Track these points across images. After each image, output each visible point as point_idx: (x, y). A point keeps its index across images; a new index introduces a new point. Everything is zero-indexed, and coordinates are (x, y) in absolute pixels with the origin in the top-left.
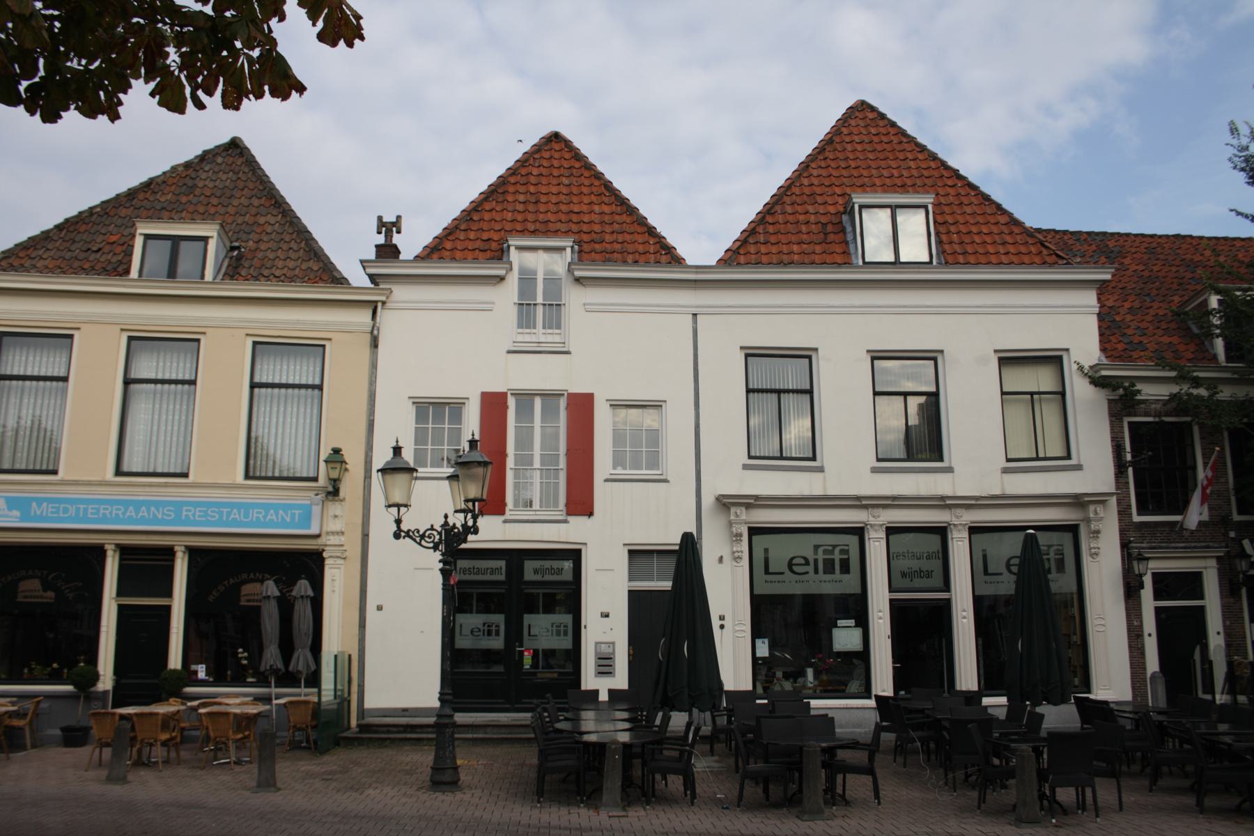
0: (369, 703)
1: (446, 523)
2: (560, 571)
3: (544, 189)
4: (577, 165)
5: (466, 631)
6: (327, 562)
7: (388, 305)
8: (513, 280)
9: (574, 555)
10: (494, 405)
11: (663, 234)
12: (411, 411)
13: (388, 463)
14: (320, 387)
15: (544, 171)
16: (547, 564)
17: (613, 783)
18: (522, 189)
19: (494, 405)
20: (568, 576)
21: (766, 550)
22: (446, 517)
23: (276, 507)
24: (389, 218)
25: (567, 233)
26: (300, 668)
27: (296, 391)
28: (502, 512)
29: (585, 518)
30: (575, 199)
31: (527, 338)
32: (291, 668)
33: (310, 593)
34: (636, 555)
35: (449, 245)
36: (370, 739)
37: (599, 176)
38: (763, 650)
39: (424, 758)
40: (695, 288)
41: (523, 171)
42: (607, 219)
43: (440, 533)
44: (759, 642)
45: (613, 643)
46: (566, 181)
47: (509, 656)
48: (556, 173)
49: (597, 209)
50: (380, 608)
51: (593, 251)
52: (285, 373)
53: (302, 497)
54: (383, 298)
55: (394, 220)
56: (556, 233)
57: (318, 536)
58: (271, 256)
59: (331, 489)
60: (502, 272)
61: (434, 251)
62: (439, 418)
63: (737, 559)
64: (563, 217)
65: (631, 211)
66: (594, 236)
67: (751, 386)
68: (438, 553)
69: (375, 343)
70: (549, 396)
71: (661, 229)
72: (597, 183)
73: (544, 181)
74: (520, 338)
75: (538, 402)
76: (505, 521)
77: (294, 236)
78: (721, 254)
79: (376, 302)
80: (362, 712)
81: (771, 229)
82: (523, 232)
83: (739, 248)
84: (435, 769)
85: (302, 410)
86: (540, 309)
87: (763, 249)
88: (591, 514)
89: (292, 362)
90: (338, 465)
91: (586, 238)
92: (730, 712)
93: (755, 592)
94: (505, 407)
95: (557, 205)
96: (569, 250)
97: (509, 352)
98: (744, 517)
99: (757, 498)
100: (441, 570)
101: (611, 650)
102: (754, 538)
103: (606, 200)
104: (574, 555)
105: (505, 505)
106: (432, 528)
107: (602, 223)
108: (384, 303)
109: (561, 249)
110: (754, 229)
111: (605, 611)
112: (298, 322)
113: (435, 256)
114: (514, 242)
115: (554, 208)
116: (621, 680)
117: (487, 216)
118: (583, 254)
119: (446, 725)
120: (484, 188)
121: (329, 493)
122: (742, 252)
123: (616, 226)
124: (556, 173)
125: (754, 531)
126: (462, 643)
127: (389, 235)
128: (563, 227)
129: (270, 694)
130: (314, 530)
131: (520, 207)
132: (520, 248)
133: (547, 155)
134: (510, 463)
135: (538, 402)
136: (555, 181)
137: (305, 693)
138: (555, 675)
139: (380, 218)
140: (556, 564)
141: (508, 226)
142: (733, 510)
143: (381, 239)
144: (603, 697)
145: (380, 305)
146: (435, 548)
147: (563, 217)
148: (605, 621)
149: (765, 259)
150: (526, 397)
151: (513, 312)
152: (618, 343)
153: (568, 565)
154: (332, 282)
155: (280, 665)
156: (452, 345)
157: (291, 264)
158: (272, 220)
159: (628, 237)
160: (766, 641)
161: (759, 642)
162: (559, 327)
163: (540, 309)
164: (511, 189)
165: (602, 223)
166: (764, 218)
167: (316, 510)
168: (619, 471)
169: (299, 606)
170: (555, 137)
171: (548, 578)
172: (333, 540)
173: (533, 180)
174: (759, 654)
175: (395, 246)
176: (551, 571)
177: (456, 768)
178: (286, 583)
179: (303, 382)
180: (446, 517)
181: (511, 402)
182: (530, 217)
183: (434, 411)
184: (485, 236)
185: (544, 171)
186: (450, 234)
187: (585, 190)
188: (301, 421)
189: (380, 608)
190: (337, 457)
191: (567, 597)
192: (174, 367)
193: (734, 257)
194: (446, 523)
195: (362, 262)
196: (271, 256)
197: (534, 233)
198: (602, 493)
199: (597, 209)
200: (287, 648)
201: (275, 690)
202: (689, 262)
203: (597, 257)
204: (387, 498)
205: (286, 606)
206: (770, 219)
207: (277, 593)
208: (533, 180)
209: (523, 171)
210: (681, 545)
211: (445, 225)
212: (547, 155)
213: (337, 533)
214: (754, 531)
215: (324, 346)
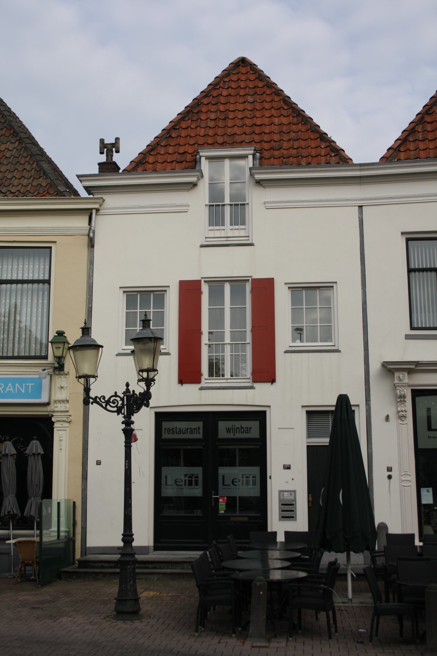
0: (90, 543)
1: (128, 390)
2: (248, 430)
3: (232, 108)
4: (261, 84)
5: (170, 481)
6: (55, 425)
7: (101, 212)
8: (204, 187)
9: (260, 417)
10: (190, 291)
11: (333, 138)
12: (122, 299)
13: (77, 341)
14: (48, 282)
15: (233, 92)
16: (238, 424)
17: (258, 616)
18: (213, 108)
19: (190, 291)
20: (255, 434)
21: (429, 410)
22: (127, 385)
23: (14, 381)
24: (109, 140)
25: (250, 143)
26: (32, 514)
27: (30, 285)
28: (199, 382)
29: (270, 384)
30: (258, 114)
31: (217, 234)
32: (25, 514)
33: (41, 451)
34: (313, 415)
35: (151, 159)
36: (86, 573)
37: (279, 92)
38: (428, 497)
39: (112, 589)
40: (360, 184)
41: (215, 93)
42: (285, 129)
43: (122, 399)
44: (424, 491)
45: (295, 491)
46: (250, 99)
47: (205, 503)
48: (242, 92)
49: (276, 121)
50: (99, 463)
51: (273, 157)
52: (20, 271)
53: (32, 371)
54: (97, 206)
55: (114, 142)
56: (241, 144)
57: (48, 404)
58: (9, 176)
59: (57, 365)
60: (194, 179)
61: (140, 164)
62: (145, 304)
63: (402, 417)
64: (248, 130)
65: (306, 121)
66: (273, 144)
67: (412, 267)
68: (121, 416)
69: (91, 244)
70: (237, 283)
71: (332, 135)
72: (277, 99)
73: (232, 100)
74: (211, 234)
75: (227, 288)
76: (201, 389)
77: (28, 159)
78: (383, 152)
79: (92, 209)
80: (85, 549)
81: (429, 128)
82: (214, 145)
83: (399, 146)
84: (120, 601)
85: (35, 301)
86: (227, 209)
87: (422, 146)
88: (273, 381)
89: (26, 263)
90: (61, 346)
91: (266, 146)
92: (385, 552)
93: (420, 447)
94: (199, 293)
95: (246, 121)
96: (251, 157)
97: (202, 246)
98: (406, 381)
99: (417, 363)
100: (123, 430)
101: (292, 498)
102: (417, 399)
103: (285, 113)
104: (260, 417)
105: (200, 375)
106: (116, 395)
107: (281, 132)
108: (97, 210)
109: (244, 157)
110: (413, 128)
111: (287, 463)
112: (29, 229)
113: (140, 169)
114: (204, 153)
115: (239, 123)
116: (301, 524)
117: (183, 133)
118: (264, 160)
119: (127, 563)
120: (181, 109)
121: (55, 369)
122: (402, 149)
123: (293, 135)
124: (242, 92)
125: (416, 393)
126: (169, 491)
127: (110, 155)
128: (247, 138)
129: (9, 535)
130: (44, 399)
131: (212, 124)
132: (208, 158)
133: (235, 78)
134: (205, 339)
135: (227, 288)
136: (241, 100)
137: (32, 535)
138: (246, 519)
139: (102, 141)
140: (246, 424)
141: (201, 140)
142: (396, 374)
143: (103, 158)
144: (281, 538)
145: (94, 212)
146: (119, 411)
147: (248, 130)
148: (287, 470)
149: (422, 154)
150: (216, 284)
151: (204, 214)
152: (295, 235)
153: (255, 425)
154: (57, 195)
155: (16, 511)
156: (154, 243)
157: (25, 182)
158: (11, 147)
159: (303, 144)
160: (431, 490)
161: (424, 491)
162: (243, 223)
163: (227, 209)
164: (204, 109)
165: (281, 132)
166: (422, 118)
167: (46, 382)
168: (298, 343)
169: (31, 462)
170: (242, 62)
171: (238, 435)
172: (60, 407)
173: (223, 100)
174: (424, 502)
175: (115, 163)
176: (241, 430)
177: (137, 600)
178: (21, 444)
179: (36, 278)
180: (127, 385)
181: (205, 288)
182: (220, 131)
183: (142, 299)
184: (181, 150)
185: (233, 92)
186: (152, 150)
187: (267, 106)
188: (35, 310)
189: (99, 463)
190: (61, 339)
191: (255, 453)
192: (30, 269)
193: (394, 154)
194: (128, 390)
195: (77, 175)
196: (9, 176)
197: (223, 145)
198: (282, 361)
199: (276, 121)
200: (22, 497)
201: (12, 532)
202: (355, 161)
203: (276, 161)
204: (77, 371)
205: (22, 462)
206: (428, 119)
207: (14, 451)
208: (223, 100)
209: (215, 93)
210: (337, 406)
211: (148, 142)
212: (235, 78)
213: (63, 401)
214: (416, 393)
215: (50, 248)
